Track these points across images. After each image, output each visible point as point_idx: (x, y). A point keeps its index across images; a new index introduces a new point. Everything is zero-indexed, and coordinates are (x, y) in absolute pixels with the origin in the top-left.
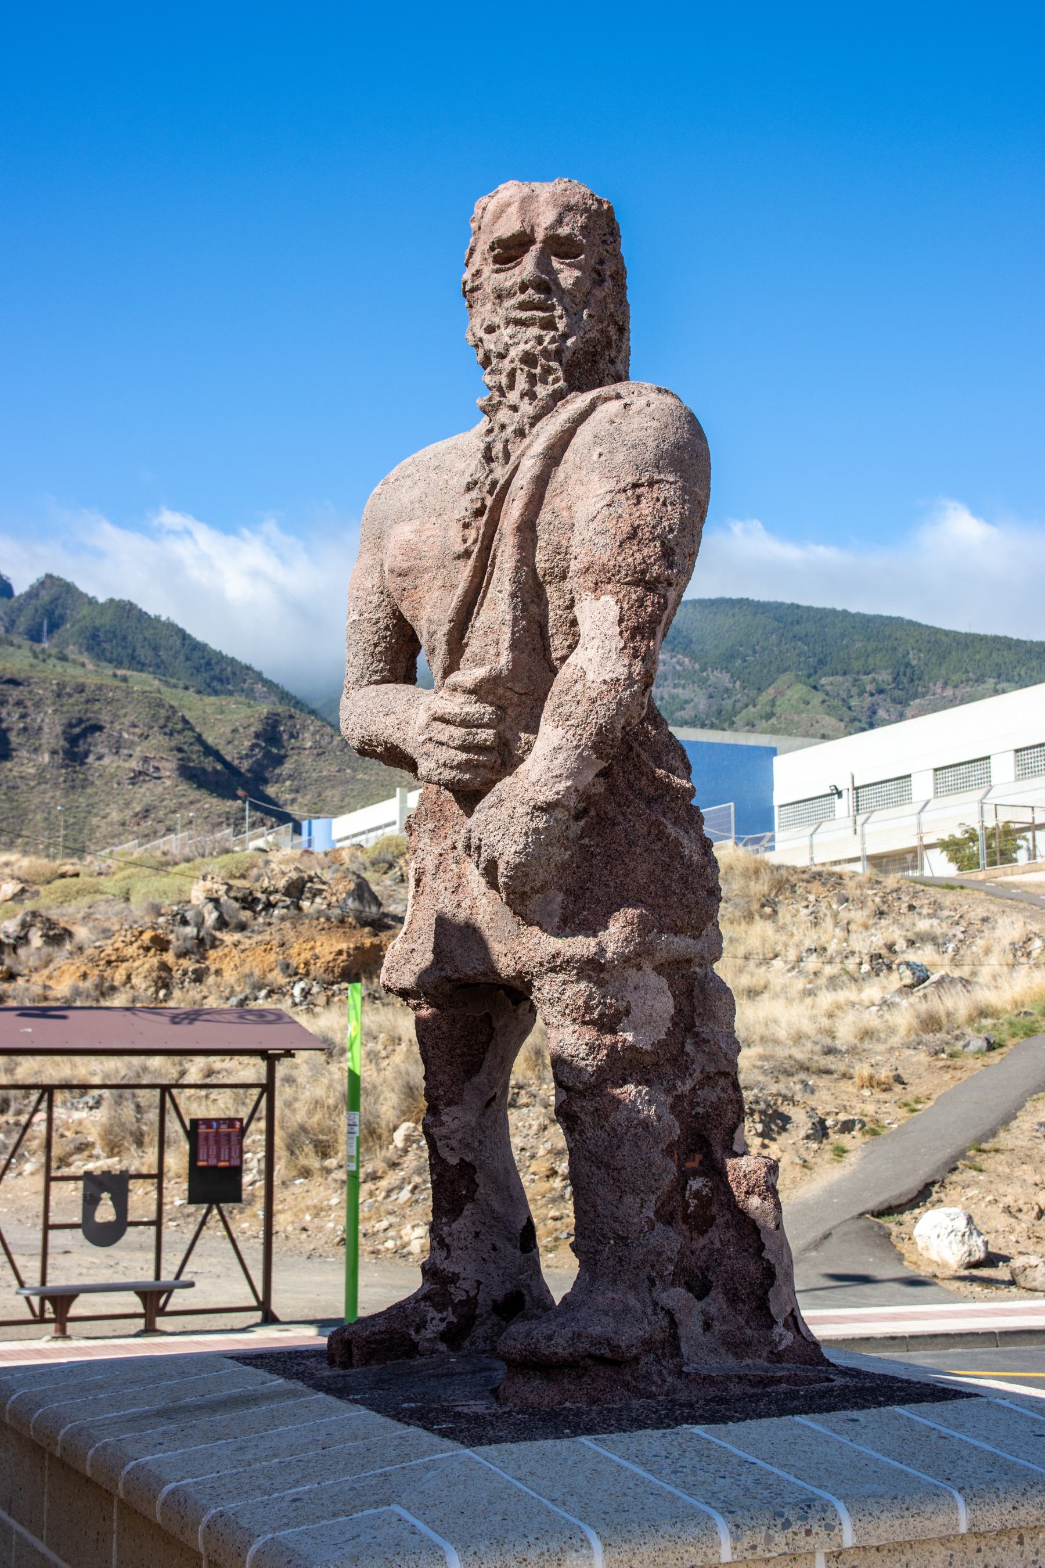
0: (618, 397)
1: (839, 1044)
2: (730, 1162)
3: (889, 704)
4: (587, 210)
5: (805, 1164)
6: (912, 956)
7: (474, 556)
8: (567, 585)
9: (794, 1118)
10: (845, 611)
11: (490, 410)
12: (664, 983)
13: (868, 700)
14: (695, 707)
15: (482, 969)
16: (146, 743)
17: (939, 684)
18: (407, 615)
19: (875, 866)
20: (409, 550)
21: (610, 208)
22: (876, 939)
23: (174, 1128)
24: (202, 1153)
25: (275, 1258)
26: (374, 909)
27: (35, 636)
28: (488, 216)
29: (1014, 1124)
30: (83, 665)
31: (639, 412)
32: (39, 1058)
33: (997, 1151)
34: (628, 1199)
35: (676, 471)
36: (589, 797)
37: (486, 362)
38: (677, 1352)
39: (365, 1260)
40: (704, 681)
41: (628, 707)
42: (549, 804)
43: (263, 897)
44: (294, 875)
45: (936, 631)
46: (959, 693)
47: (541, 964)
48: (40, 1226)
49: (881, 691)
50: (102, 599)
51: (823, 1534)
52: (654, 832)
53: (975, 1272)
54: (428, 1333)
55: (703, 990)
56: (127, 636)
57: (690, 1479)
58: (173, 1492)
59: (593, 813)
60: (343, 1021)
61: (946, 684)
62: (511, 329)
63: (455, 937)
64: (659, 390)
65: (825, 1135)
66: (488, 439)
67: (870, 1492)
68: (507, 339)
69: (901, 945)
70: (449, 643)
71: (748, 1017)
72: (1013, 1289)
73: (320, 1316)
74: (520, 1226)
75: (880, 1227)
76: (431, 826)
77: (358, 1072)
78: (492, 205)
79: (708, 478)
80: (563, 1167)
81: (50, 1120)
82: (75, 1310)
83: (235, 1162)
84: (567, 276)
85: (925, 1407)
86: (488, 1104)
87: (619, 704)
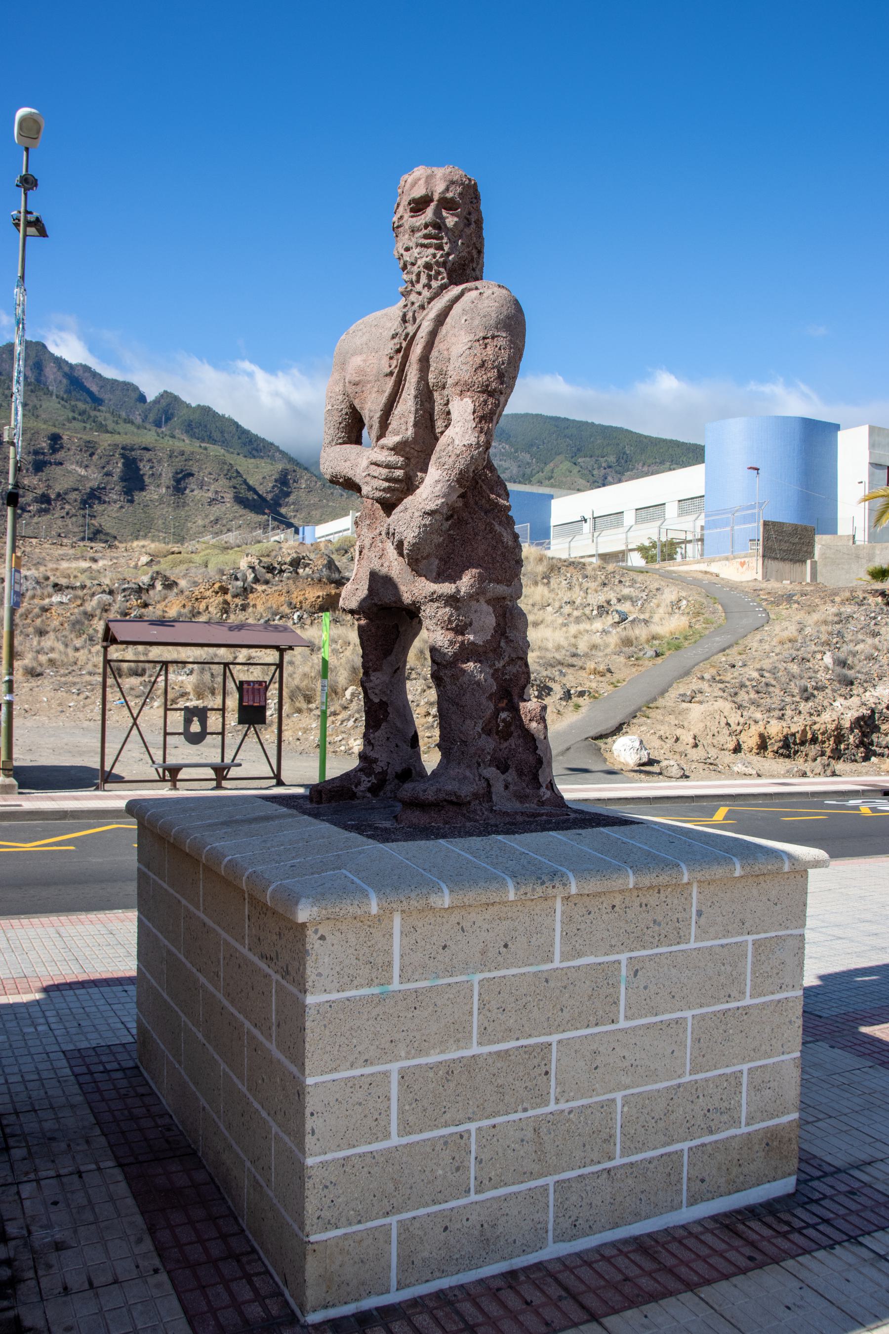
0: (477, 289)
1: (579, 652)
2: (522, 704)
3: (614, 474)
4: (463, 184)
5: (559, 712)
6: (619, 608)
7: (395, 375)
8: (446, 392)
9: (554, 689)
10: (593, 423)
11: (406, 294)
12: (491, 609)
13: (603, 471)
14: (511, 472)
15: (393, 599)
16: (217, 483)
17: (641, 464)
18: (358, 407)
19: (602, 559)
20: (360, 371)
21: (475, 184)
22: (601, 598)
23: (231, 685)
24: (245, 699)
25: (283, 754)
26: (337, 575)
27: (158, 424)
28: (408, 185)
29: (667, 694)
30: (184, 441)
31: (488, 298)
32: (161, 648)
33: (657, 708)
34: (468, 722)
35: (507, 331)
36: (454, 509)
37: (404, 268)
38: (490, 800)
39: (329, 755)
40: (516, 458)
41: (476, 460)
42: (432, 511)
43: (278, 567)
44: (295, 555)
45: (641, 435)
46: (651, 469)
47: (426, 597)
48: (162, 734)
49: (610, 467)
50: (193, 405)
51: (561, 887)
52: (488, 528)
53: (642, 768)
54: (362, 788)
55: (511, 614)
56: (208, 425)
57: (495, 861)
58: (230, 861)
59: (455, 517)
60: (319, 633)
61: (644, 464)
62: (418, 250)
63: (380, 582)
64: (499, 286)
65: (570, 698)
66: (404, 310)
67: (585, 867)
68: (416, 255)
69: (614, 601)
70: (380, 422)
71: (532, 635)
72: (660, 776)
73: (306, 783)
74: (411, 735)
75: (596, 745)
76: (368, 522)
77: (327, 658)
78: (410, 179)
79: (524, 336)
80: (434, 711)
81: (166, 680)
82: (180, 776)
83: (262, 704)
84: (451, 221)
85: (616, 828)
86: (395, 671)
87: (472, 458)
